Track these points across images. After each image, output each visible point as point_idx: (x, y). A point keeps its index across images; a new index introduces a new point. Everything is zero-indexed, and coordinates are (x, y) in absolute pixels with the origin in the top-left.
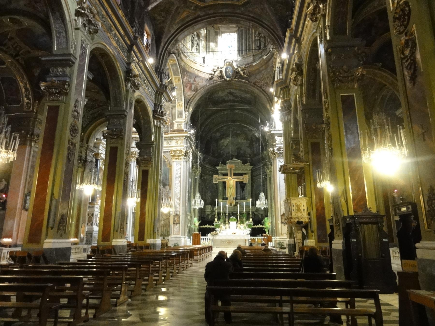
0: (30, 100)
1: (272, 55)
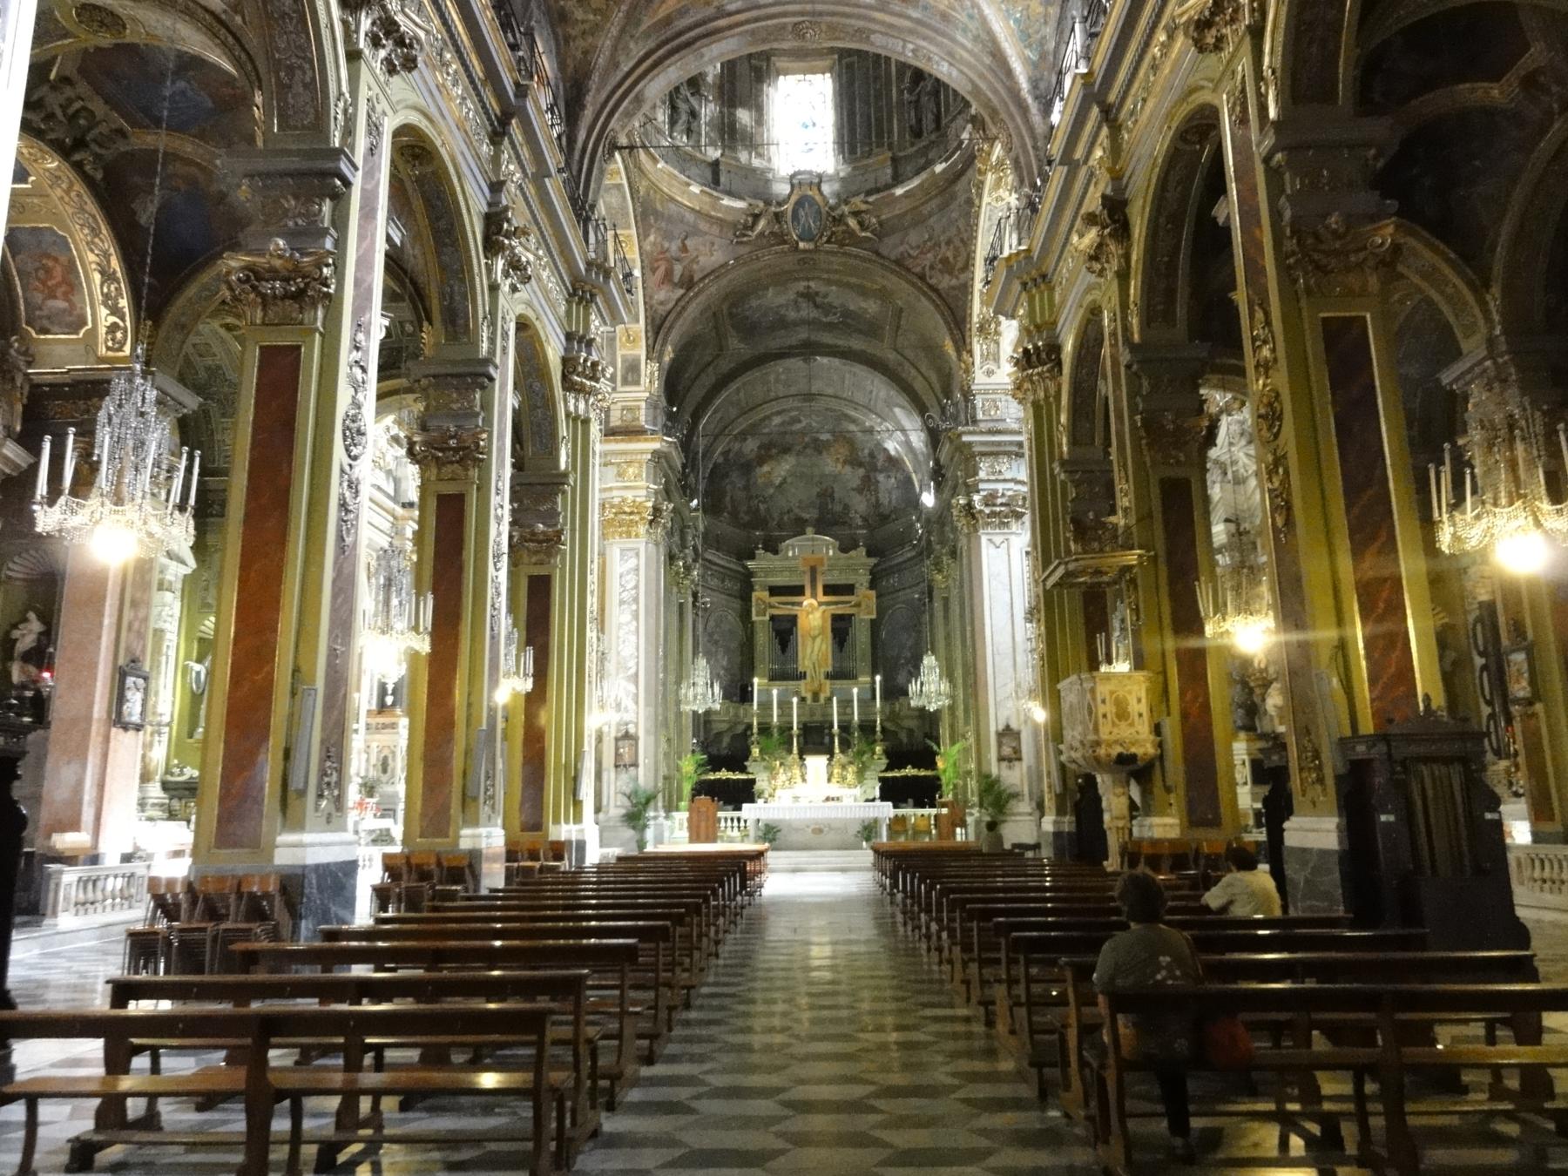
0: (123, 320)
1: (970, 160)
